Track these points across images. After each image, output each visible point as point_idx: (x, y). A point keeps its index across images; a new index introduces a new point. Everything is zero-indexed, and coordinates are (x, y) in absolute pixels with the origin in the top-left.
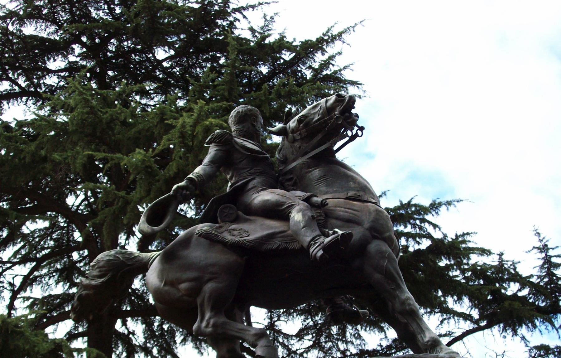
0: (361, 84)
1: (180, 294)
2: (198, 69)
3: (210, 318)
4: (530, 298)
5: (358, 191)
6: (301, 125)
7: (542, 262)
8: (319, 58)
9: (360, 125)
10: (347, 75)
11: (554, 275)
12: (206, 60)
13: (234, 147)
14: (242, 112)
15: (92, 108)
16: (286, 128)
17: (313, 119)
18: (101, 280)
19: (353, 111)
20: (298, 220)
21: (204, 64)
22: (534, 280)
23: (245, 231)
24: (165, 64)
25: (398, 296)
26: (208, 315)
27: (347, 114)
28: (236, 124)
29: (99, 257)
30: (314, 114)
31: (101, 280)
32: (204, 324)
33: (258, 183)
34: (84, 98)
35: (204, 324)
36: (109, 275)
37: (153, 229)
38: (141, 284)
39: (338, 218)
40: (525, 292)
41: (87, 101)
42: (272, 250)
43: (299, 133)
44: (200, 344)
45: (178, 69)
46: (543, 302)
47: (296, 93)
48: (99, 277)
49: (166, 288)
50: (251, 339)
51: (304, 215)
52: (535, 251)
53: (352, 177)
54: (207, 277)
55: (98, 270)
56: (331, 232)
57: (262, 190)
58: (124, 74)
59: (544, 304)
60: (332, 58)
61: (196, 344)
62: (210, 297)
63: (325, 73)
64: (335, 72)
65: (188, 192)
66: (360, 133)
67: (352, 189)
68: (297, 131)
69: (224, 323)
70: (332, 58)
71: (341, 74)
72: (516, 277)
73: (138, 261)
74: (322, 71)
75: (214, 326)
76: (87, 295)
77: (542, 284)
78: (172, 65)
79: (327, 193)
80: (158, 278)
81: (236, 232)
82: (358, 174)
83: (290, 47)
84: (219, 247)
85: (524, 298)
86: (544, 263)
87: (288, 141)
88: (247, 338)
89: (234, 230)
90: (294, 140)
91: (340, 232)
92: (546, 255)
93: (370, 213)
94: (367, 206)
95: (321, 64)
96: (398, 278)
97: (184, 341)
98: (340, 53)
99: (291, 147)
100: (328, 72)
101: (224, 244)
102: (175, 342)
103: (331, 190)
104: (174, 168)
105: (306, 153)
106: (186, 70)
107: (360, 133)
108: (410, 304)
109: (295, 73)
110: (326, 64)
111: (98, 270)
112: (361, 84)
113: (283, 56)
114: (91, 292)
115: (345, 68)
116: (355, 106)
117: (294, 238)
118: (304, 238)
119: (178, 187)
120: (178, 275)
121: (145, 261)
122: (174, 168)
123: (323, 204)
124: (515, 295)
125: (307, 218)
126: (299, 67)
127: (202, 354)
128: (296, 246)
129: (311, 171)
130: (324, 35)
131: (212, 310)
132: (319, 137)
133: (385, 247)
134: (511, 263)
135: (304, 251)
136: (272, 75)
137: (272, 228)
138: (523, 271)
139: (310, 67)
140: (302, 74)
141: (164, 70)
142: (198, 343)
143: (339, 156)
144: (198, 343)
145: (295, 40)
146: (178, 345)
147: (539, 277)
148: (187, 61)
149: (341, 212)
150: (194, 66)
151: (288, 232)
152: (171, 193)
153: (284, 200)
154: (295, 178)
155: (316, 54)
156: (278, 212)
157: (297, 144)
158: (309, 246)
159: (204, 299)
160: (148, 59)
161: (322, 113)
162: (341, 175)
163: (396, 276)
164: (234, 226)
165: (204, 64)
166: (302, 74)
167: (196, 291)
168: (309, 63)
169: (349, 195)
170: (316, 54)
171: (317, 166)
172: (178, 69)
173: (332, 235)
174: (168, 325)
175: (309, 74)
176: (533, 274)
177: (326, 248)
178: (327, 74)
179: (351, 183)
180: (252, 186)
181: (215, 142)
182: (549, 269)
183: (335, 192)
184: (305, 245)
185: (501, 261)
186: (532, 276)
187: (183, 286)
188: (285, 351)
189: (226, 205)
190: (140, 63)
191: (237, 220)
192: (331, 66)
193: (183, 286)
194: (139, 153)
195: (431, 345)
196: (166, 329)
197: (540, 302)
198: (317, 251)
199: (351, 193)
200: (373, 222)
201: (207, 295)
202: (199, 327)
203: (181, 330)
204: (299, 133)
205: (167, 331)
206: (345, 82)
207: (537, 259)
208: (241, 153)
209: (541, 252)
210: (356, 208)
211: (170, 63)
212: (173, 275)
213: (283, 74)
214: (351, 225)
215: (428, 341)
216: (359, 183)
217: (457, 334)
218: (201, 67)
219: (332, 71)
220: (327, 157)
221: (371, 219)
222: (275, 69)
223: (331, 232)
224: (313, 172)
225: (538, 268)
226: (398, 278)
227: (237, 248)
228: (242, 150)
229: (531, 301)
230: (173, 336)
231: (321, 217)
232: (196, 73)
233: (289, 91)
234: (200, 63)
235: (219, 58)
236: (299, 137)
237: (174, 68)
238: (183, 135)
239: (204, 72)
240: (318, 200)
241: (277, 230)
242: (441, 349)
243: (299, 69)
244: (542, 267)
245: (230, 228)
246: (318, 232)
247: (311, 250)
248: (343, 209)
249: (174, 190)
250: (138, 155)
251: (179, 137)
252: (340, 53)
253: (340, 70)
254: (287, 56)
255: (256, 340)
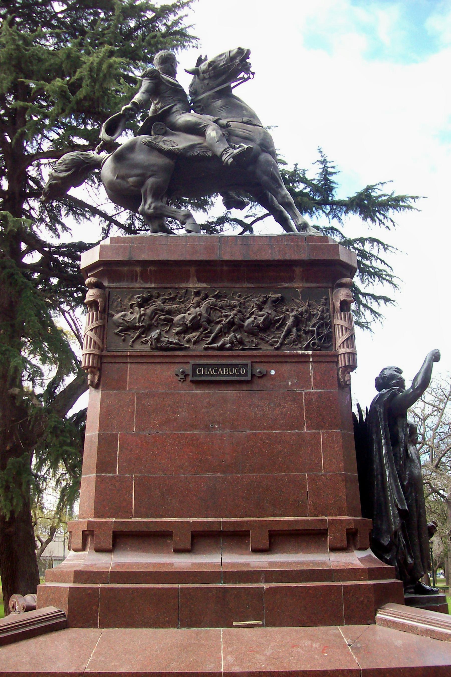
0: (199, 39)
1: (129, 185)
2: (84, 21)
3: (151, 203)
4: (311, 194)
5: (250, 117)
6: (210, 68)
7: (321, 170)
8: (172, 17)
9: (252, 71)
10: (190, 32)
11: (328, 180)
12: (90, 14)
13: (161, 81)
14: (165, 55)
15: (18, 45)
16: (198, 69)
17: (219, 64)
18: (67, 173)
19: (248, 61)
20: (213, 136)
21: (88, 17)
22: (314, 182)
23: (174, 142)
24: (60, 16)
25: (280, 193)
26: (149, 201)
27: (244, 63)
28: (160, 64)
29: (64, 156)
30: (220, 60)
31: (67, 173)
32: (147, 207)
33: (180, 108)
34: (13, 38)
35: (147, 207)
36: (73, 170)
37: (110, 138)
38: (37, 174)
39: (237, 136)
40: (308, 190)
41: (14, 40)
42: (194, 157)
43: (208, 73)
44: (78, 217)
45: (69, 19)
46: (318, 197)
47: (161, 43)
48: (66, 171)
49: (119, 181)
50: (182, 218)
51: (217, 133)
52: (318, 163)
53: (245, 107)
54: (149, 173)
55: (64, 166)
56: (237, 146)
57: (183, 113)
58: (27, 21)
59: (319, 198)
60: (181, 18)
61: (76, 217)
62: (151, 188)
63: (175, 29)
64: (182, 29)
65: (133, 112)
66: (251, 76)
67: (245, 116)
68: (207, 72)
69: (162, 207)
70: (181, 18)
71: (186, 31)
72: (304, 180)
73: (93, 160)
74: (173, 28)
75: (155, 208)
76: (56, 184)
77: (319, 185)
78: (64, 16)
79: (227, 118)
80: (111, 173)
81: (168, 143)
82: (247, 106)
83: (153, 9)
84: (156, 153)
85: (307, 194)
86: (323, 171)
87: (199, 79)
88: (178, 217)
89: (166, 141)
90: (204, 79)
91: (246, 146)
92: (325, 166)
93: (260, 134)
94: (258, 129)
95: (173, 23)
96: (280, 180)
97: (67, 214)
98: (187, 16)
99: (201, 83)
100: (177, 29)
101: (160, 151)
102: (61, 215)
103: (230, 115)
104: (84, 92)
105: (213, 88)
106: (74, 21)
107: (251, 76)
108: (288, 198)
109: (154, 27)
110: (176, 23)
111: (64, 166)
112: (199, 39)
113: (147, 15)
114: (60, 182)
115: (189, 27)
116: (250, 56)
117: (209, 148)
118: (218, 149)
119: (126, 108)
120: (127, 171)
121: (98, 160)
122: (84, 92)
123: (227, 126)
124: (301, 191)
125: (219, 135)
126: (157, 23)
127: (80, 223)
128: (210, 154)
129: (215, 101)
130: (178, 2)
131: (153, 197)
132: (224, 77)
133: (270, 158)
134: (302, 170)
135: (217, 158)
136: (137, 28)
137: (192, 141)
138: (309, 176)
139: (165, 24)
140: (159, 29)
141: (58, 20)
142: (77, 216)
143: (235, 92)
144: (77, 216)
145: (157, 3)
146: (63, 217)
147: (318, 180)
148: (76, 14)
149: (239, 132)
150: (80, 18)
151: (204, 144)
152: (121, 112)
153: (200, 121)
154: (202, 105)
155: (170, 15)
156: (196, 130)
157: (206, 82)
158: (222, 155)
159: (146, 190)
160: (47, 11)
161: (226, 60)
162: (235, 106)
163: (279, 178)
164: (165, 138)
165: (88, 17)
166: (159, 29)
167: (141, 183)
168: (164, 21)
169: (244, 120)
170: (170, 15)
171: (220, 98)
172: (69, 19)
173: (238, 148)
174: (56, 203)
175: (163, 29)
176: (315, 178)
177: (236, 157)
178: (176, 31)
179: (245, 111)
180: (176, 110)
181: (148, 77)
182: (325, 175)
183: (233, 117)
184: (219, 154)
185: (296, 169)
186: (314, 179)
187: (131, 180)
188: (140, 223)
189: (157, 123)
190: (41, 13)
191: (165, 134)
192: (179, 24)
193: (131, 180)
194: (59, 81)
195: (303, 226)
196: (55, 206)
197: (317, 197)
198: (227, 159)
199: (245, 119)
200: (262, 140)
201: (149, 186)
202: (143, 209)
203: (65, 207)
204: (208, 73)
205: (55, 208)
206: (188, 36)
207: (318, 168)
208: (167, 85)
209: (322, 164)
210: (250, 130)
211: (63, 14)
212: (123, 172)
213: (145, 28)
214: (247, 141)
215: (301, 224)
216: (250, 112)
217: (259, 216)
218: (86, 19)
219: (180, 28)
220: (226, 93)
221: (261, 138)
222: (140, 24)
223: (237, 146)
224: (217, 102)
225: (319, 174)
226: (280, 180)
227: (169, 154)
228: (167, 84)
229: (311, 196)
230: (59, 211)
231: (228, 134)
232: (82, 24)
233: (157, 41)
234: (85, 16)
235: (100, 13)
236: (208, 76)
237: (66, 18)
238: (91, 70)
239: (88, 22)
240: (224, 122)
241: (196, 142)
242: (310, 229)
243: (157, 25)
244: (321, 174)
245: (163, 139)
246: (228, 146)
247: (224, 158)
248: (240, 130)
249: (123, 111)
250: (58, 82)
251: (89, 71)
252: (187, 16)
253: (186, 28)
254: (150, 15)
255: (185, 219)
